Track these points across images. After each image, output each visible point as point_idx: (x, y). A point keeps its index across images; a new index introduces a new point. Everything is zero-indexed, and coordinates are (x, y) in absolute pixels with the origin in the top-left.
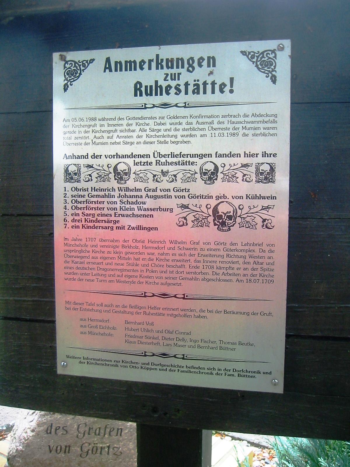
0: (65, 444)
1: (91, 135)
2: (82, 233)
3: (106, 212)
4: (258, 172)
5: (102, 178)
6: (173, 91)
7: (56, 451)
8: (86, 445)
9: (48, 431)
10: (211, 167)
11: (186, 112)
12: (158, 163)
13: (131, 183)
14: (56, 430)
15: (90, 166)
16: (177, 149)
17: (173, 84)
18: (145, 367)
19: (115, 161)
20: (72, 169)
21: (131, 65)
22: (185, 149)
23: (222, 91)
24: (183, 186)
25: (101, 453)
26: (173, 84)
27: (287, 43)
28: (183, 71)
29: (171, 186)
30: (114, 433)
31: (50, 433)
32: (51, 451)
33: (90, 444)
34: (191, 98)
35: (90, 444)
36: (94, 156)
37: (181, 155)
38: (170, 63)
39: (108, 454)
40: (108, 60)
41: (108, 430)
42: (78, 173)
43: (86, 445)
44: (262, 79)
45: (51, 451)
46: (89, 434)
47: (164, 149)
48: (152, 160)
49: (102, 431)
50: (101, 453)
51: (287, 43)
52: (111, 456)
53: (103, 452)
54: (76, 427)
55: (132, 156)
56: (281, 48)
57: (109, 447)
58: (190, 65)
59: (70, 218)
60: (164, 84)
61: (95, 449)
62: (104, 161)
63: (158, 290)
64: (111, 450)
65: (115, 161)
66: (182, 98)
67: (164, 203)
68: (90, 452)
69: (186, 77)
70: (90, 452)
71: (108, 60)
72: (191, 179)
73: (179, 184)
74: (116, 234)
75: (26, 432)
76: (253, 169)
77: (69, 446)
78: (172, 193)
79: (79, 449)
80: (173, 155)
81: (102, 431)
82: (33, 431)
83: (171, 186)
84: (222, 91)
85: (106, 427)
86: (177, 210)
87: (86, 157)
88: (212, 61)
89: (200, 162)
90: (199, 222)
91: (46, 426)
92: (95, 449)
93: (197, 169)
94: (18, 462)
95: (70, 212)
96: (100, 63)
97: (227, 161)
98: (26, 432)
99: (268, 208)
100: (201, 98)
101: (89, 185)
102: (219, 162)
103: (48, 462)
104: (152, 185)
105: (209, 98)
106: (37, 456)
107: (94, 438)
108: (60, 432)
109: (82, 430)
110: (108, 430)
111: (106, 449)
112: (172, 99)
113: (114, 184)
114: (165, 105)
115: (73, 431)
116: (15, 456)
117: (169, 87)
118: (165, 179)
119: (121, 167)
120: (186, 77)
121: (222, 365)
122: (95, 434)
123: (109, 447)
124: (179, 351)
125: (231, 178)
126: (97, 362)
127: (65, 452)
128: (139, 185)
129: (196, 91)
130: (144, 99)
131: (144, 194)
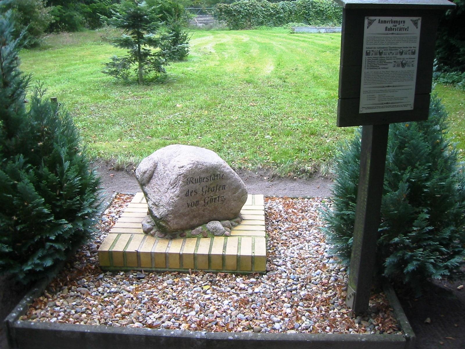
0: (196, 200)
1: (374, 42)
2: (369, 70)
3: (376, 64)
4: (412, 52)
5: (376, 54)
6: (395, 30)
7: (192, 205)
8: (207, 198)
9: (187, 195)
10: (402, 51)
11: (397, 36)
12: (390, 50)
13: (383, 56)
14: (191, 193)
15: (373, 51)
16: (394, 46)
17: (395, 28)
18: (382, 107)
19: (379, 50)
20: (368, 52)
21: (385, 22)
22: (396, 46)
23: (406, 30)
24: (395, 56)
25: (215, 202)
26: (395, 28)
27: (420, 18)
28: (397, 24)
29: (392, 56)
30: (221, 189)
31: (188, 195)
32: (188, 207)
33: (209, 198)
34: (399, 32)
35: (209, 198)
36: (375, 48)
37: (395, 48)
38: (395, 22)
39: (219, 201)
40: (379, 20)
41: (218, 187)
42: (369, 53)
43: (207, 198)
44: (415, 27)
45: (188, 207)
46: (208, 192)
47: (392, 46)
48: (388, 49)
49: (215, 189)
50: (215, 202)
51: (420, 18)
52: (220, 202)
53: (216, 201)
54: (201, 189)
55: (384, 48)
56: (419, 19)
57: (219, 197)
58: (399, 23)
59: (366, 66)
60: (393, 28)
61: (211, 200)
62: (376, 49)
63: (387, 85)
64: (220, 198)
65: (379, 50)
66: (397, 32)
67: (390, 61)
68: (209, 202)
69: (398, 26)
70: (209, 202)
71: (379, 20)
72: (397, 54)
73: (394, 56)
74: (378, 70)
75: (173, 199)
76: (411, 51)
77: (198, 201)
78: (392, 58)
79: (203, 202)
80: (394, 48)
81: (215, 189)
82: (178, 196)
83: (392, 56)
84: (406, 30)
85: (217, 186)
86: (393, 63)
87: (372, 48)
88: (404, 22)
89: (399, 49)
90: (398, 66)
91: (185, 192)
92: (211, 200)
93: (398, 51)
94: (170, 217)
95: (367, 64)
96: (377, 21)
97: (406, 49)
98: (173, 199)
99: (413, 61)
100: (401, 32)
101: (372, 56)
102: (404, 49)
103: (187, 213)
104: (388, 56)
105: (403, 32)
106: (181, 211)
107: (211, 193)
108: (193, 194)
109: (204, 190)
110: (218, 187)
111: (218, 199)
112: (394, 32)
113: (378, 56)
114: (393, 34)
115: (200, 192)
116: (167, 215)
117: (394, 29)
118: (391, 54)
119: (381, 51)
120: (398, 26)
121: (402, 104)
122: (212, 191)
123: (219, 197)
124: (390, 102)
125: (406, 54)
126: (369, 108)
127: (196, 205)
128: (385, 56)
129: (400, 30)
130: (387, 32)
131: (385, 58)
